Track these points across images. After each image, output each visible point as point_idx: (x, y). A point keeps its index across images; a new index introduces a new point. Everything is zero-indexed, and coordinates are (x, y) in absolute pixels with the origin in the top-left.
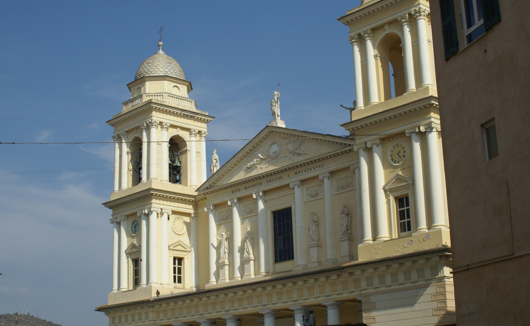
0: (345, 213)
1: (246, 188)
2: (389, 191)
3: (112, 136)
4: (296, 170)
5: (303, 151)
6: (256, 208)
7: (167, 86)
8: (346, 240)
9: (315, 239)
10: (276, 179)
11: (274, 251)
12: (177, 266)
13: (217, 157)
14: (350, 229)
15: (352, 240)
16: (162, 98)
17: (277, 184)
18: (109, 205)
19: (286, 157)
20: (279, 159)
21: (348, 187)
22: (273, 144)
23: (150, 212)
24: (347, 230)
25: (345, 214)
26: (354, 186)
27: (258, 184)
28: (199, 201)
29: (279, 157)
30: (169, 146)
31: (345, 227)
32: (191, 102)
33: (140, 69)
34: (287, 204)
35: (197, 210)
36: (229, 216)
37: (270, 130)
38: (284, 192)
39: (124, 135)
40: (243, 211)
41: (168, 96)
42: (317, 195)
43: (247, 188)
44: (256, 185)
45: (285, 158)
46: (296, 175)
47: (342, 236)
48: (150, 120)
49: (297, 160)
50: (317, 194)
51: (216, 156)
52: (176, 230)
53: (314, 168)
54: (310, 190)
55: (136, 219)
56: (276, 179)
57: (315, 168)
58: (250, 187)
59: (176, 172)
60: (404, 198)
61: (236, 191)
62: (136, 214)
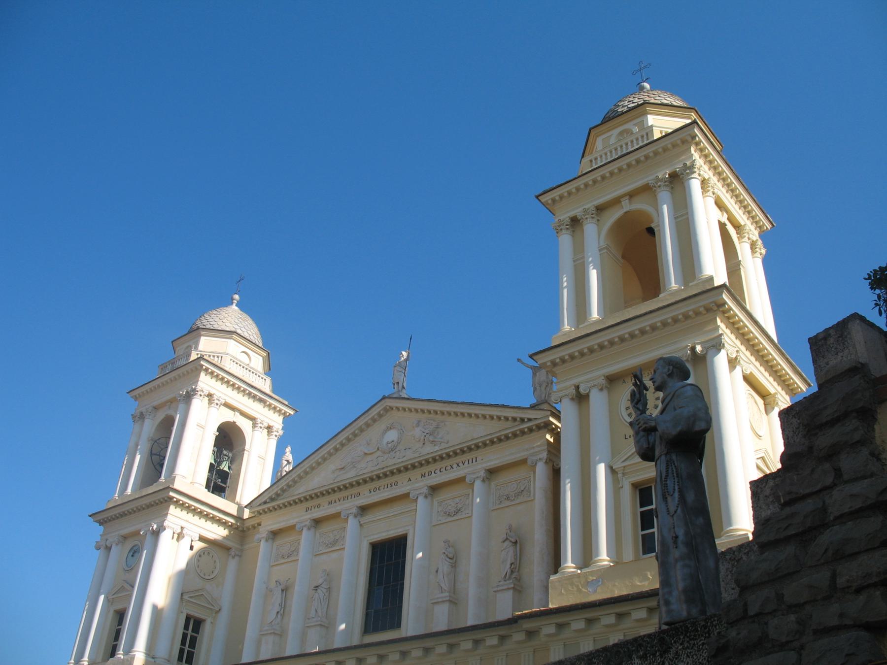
0: (511, 539)
1: (330, 503)
2: (622, 472)
3: (132, 415)
4: (425, 469)
5: (442, 438)
6: (344, 537)
7: (233, 347)
8: (509, 589)
9: (446, 589)
10: (386, 487)
11: (365, 613)
12: (190, 632)
13: (290, 458)
14: (518, 571)
15: (520, 592)
16: (219, 361)
17: (387, 494)
18: (99, 519)
19: (410, 448)
20: (395, 452)
21: (519, 497)
22: (389, 428)
23: (161, 528)
24: (512, 572)
25: (511, 541)
26: (532, 494)
27: (353, 496)
28: (248, 529)
29: (397, 450)
30: (217, 434)
31: (508, 566)
32: (265, 380)
33: (677, 101)
34: (400, 530)
35: (242, 545)
36: (293, 551)
37: (387, 406)
38: (397, 509)
39: (150, 413)
40: (320, 543)
41: (231, 360)
42: (457, 513)
43: (333, 502)
44: (349, 497)
45: (406, 450)
46: (423, 478)
47: (502, 583)
48: (194, 387)
49: (429, 450)
50: (459, 510)
51: (289, 456)
52: (201, 570)
53: (458, 465)
54: (446, 504)
55: (136, 542)
56: (386, 487)
57: (459, 465)
58: (337, 501)
59: (220, 480)
60: (651, 487)
61: (313, 507)
62: (137, 533)
